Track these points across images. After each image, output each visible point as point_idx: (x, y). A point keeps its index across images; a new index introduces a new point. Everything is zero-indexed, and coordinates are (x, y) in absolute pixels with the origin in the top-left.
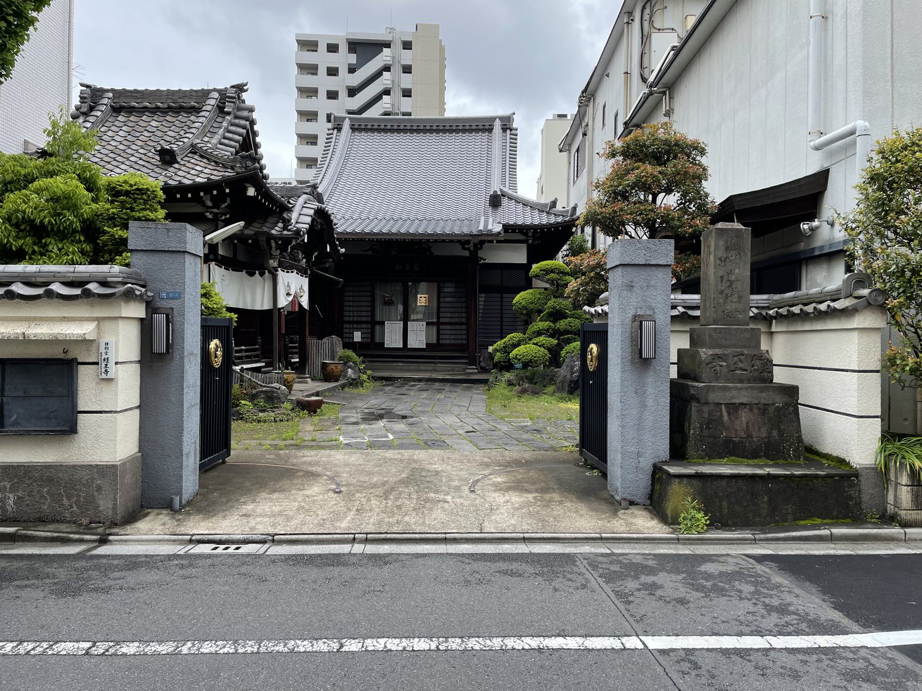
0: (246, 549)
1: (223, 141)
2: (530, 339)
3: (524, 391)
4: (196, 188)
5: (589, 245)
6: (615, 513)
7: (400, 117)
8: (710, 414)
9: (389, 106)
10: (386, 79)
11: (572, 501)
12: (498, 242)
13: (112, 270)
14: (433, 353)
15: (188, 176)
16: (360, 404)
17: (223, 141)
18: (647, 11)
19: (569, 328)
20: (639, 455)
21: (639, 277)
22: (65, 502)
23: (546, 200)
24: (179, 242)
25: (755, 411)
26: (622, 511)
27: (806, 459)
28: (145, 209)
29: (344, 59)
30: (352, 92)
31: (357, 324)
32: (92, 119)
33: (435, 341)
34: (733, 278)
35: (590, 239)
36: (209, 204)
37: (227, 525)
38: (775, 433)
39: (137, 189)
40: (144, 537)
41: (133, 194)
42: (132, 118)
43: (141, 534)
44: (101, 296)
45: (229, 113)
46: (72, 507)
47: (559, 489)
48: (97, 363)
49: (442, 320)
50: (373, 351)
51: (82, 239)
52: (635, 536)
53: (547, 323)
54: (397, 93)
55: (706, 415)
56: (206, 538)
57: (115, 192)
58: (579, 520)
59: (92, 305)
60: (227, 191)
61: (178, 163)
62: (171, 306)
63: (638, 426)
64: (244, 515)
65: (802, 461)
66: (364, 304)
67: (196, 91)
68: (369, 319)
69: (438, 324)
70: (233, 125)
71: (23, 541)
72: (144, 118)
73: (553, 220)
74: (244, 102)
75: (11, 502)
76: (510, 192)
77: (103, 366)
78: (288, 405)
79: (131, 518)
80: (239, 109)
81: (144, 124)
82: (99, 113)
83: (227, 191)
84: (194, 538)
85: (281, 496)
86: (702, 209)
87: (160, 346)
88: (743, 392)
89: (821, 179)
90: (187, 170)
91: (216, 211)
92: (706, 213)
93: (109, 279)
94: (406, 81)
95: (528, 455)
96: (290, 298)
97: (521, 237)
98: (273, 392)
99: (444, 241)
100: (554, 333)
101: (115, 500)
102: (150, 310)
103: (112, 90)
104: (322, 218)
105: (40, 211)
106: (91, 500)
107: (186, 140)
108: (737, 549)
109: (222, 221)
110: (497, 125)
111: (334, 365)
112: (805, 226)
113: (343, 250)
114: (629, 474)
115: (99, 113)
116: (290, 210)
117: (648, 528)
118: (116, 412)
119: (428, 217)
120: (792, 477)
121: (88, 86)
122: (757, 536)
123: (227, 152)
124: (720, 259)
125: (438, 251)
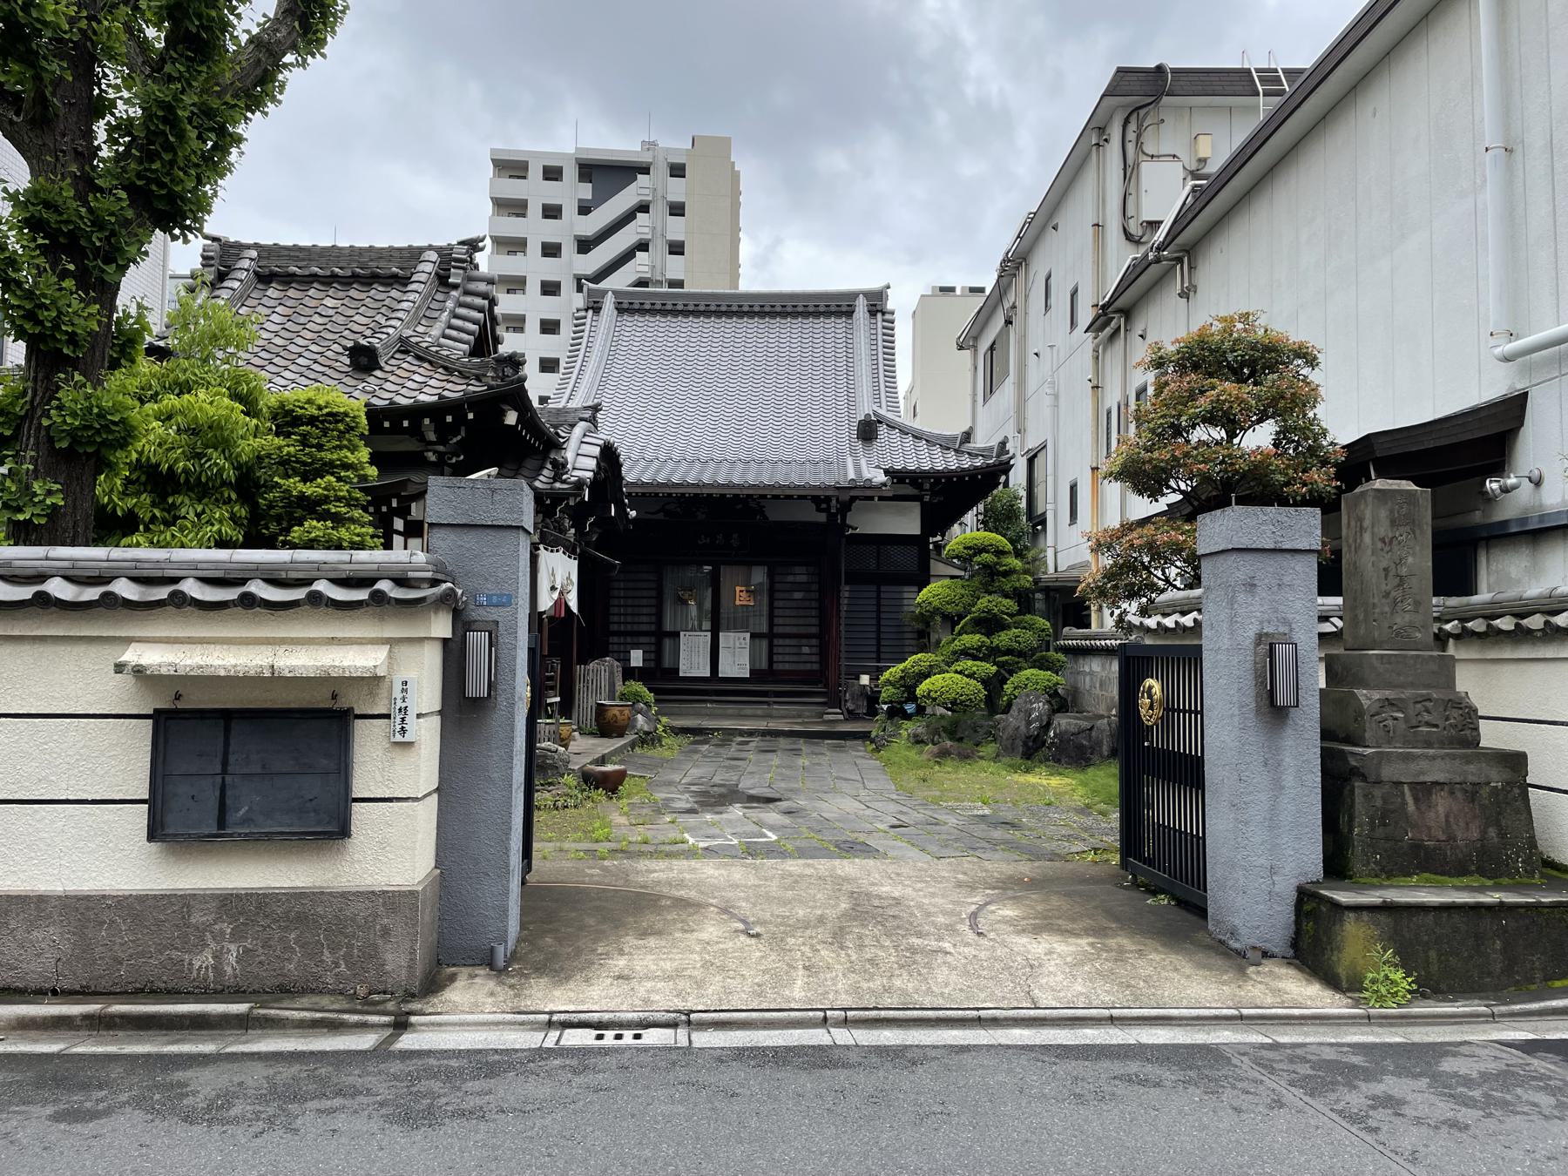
0: (652, 1037)
1: (448, 331)
2: (949, 664)
3: (944, 754)
4: (417, 412)
5: (1023, 505)
6: (1242, 971)
7: (665, 289)
8: (1385, 801)
9: (646, 269)
10: (640, 227)
11: (1156, 950)
12: (881, 498)
13: (414, 559)
14: (765, 684)
15: (404, 391)
16: (676, 777)
17: (448, 331)
18: (1132, 127)
19: (1016, 646)
20: (1273, 871)
21: (1265, 569)
22: (327, 956)
23: (956, 429)
24: (511, 511)
25: (1459, 795)
26: (1252, 969)
27: (1543, 876)
28: (340, 447)
29: (570, 191)
30: (585, 245)
31: (635, 637)
32: (225, 294)
33: (764, 665)
34: (1404, 571)
35: (1023, 493)
36: (432, 437)
37: (596, 994)
38: (1492, 832)
39: (330, 414)
40: (470, 1018)
41: (322, 422)
42: (291, 293)
43: (463, 1012)
44: (399, 602)
45: (455, 287)
46: (337, 965)
47: (1121, 929)
48: (388, 716)
49: (776, 630)
50: (663, 679)
51: (234, 496)
52: (1296, 1012)
53: (978, 636)
54: (659, 248)
55: (1379, 803)
56: (575, 1018)
57: (287, 420)
58: (1187, 987)
59: (382, 618)
60: (471, 416)
61: (381, 369)
62: (495, 617)
63: (1261, 823)
64: (619, 977)
65: (1537, 879)
66: (644, 602)
67: (400, 249)
68: (653, 628)
69: (770, 636)
70: (462, 305)
71: (262, 1027)
72: (311, 292)
73: (966, 463)
74: (477, 267)
75: (232, 959)
76: (890, 415)
77: (398, 720)
78: (569, 779)
79: (433, 985)
80: (471, 279)
81: (313, 303)
82: (236, 285)
83: (471, 416)
84: (555, 1018)
85: (663, 943)
86: (1314, 454)
87: (477, 686)
88: (1439, 763)
89: (1512, 410)
90: (399, 381)
91: (441, 448)
92: (1324, 462)
93: (411, 574)
94: (676, 229)
95: (1026, 868)
96: (556, 595)
97: (910, 491)
98: (545, 757)
99: (789, 497)
100: (991, 654)
101: (413, 952)
102: (460, 625)
103: (256, 246)
104: (609, 457)
105: (169, 450)
106: (372, 953)
107: (391, 331)
108: (1482, 1033)
109: (450, 465)
110: (861, 306)
111: (617, 711)
112: (1492, 485)
113: (633, 513)
114: (1257, 903)
115: (236, 285)
116: (559, 447)
117: (1310, 998)
118: (416, 799)
119: (717, 456)
120: (1537, 907)
121: (214, 239)
122: (1496, 1010)
123: (458, 350)
124: (1382, 540)
125: (775, 514)
